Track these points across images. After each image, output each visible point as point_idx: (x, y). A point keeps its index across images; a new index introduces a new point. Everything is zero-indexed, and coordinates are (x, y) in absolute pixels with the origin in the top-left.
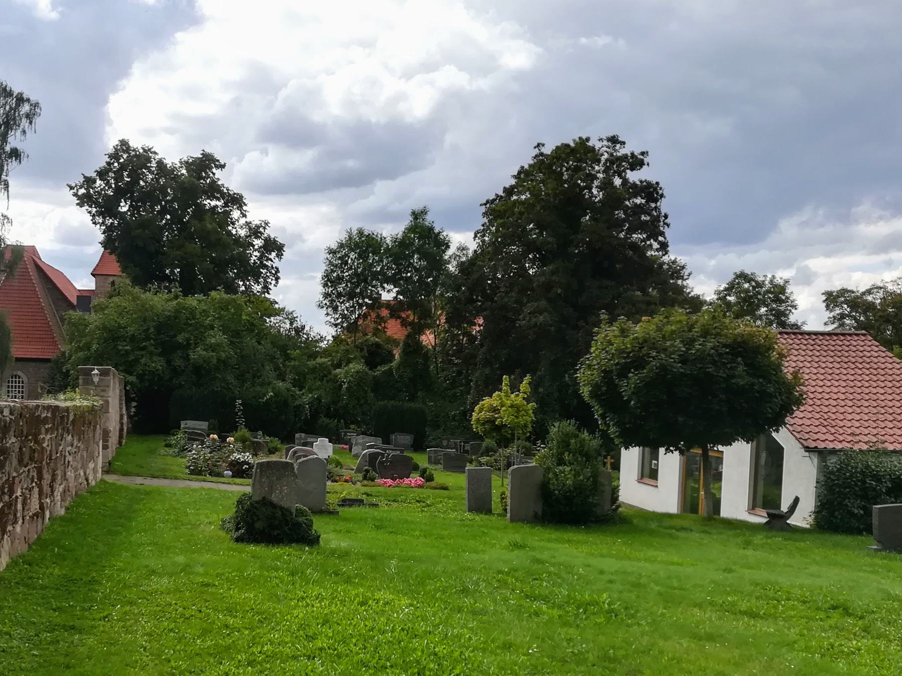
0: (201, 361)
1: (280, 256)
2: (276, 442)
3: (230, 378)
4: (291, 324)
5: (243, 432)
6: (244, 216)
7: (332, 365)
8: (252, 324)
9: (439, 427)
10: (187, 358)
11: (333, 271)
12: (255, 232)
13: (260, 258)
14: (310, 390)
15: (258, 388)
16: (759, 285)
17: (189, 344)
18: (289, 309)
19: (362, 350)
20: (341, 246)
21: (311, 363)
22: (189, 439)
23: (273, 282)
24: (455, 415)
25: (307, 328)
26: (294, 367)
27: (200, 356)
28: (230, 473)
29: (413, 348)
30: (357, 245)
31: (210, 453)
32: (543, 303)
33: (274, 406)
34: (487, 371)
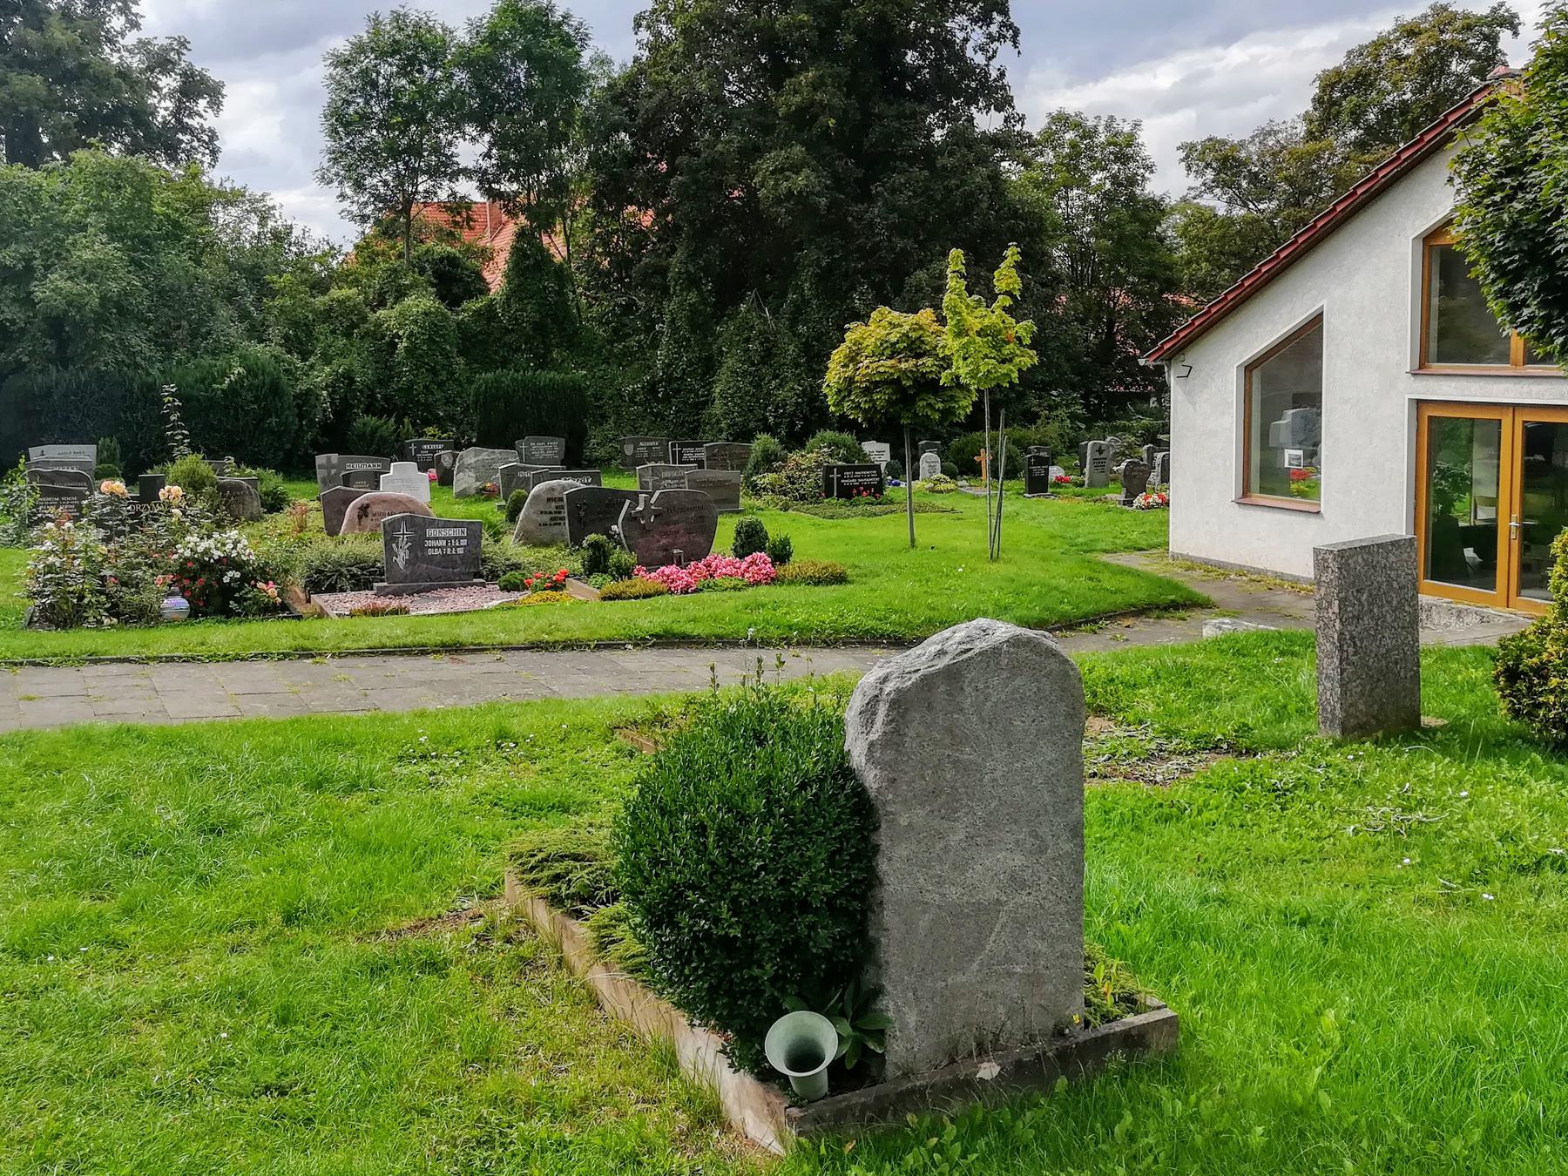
0: (60, 303)
1: (216, 104)
2: (273, 480)
3: (138, 340)
4: (263, 221)
5: (190, 462)
6: (135, 25)
7: (367, 303)
8: (176, 224)
9: (604, 417)
10: (28, 301)
11: (348, 103)
12: (162, 61)
13: (176, 113)
14: (327, 359)
15: (207, 360)
16: (1089, 134)
17: (29, 270)
18: (255, 190)
19: (422, 271)
20: (360, 49)
21: (320, 301)
22: (46, 492)
23: (207, 159)
24: (635, 392)
25: (296, 232)
26: (282, 310)
27: (56, 290)
28: (180, 603)
29: (529, 262)
30: (395, 49)
31: (107, 540)
32: (798, 150)
33: (250, 396)
34: (693, 297)
